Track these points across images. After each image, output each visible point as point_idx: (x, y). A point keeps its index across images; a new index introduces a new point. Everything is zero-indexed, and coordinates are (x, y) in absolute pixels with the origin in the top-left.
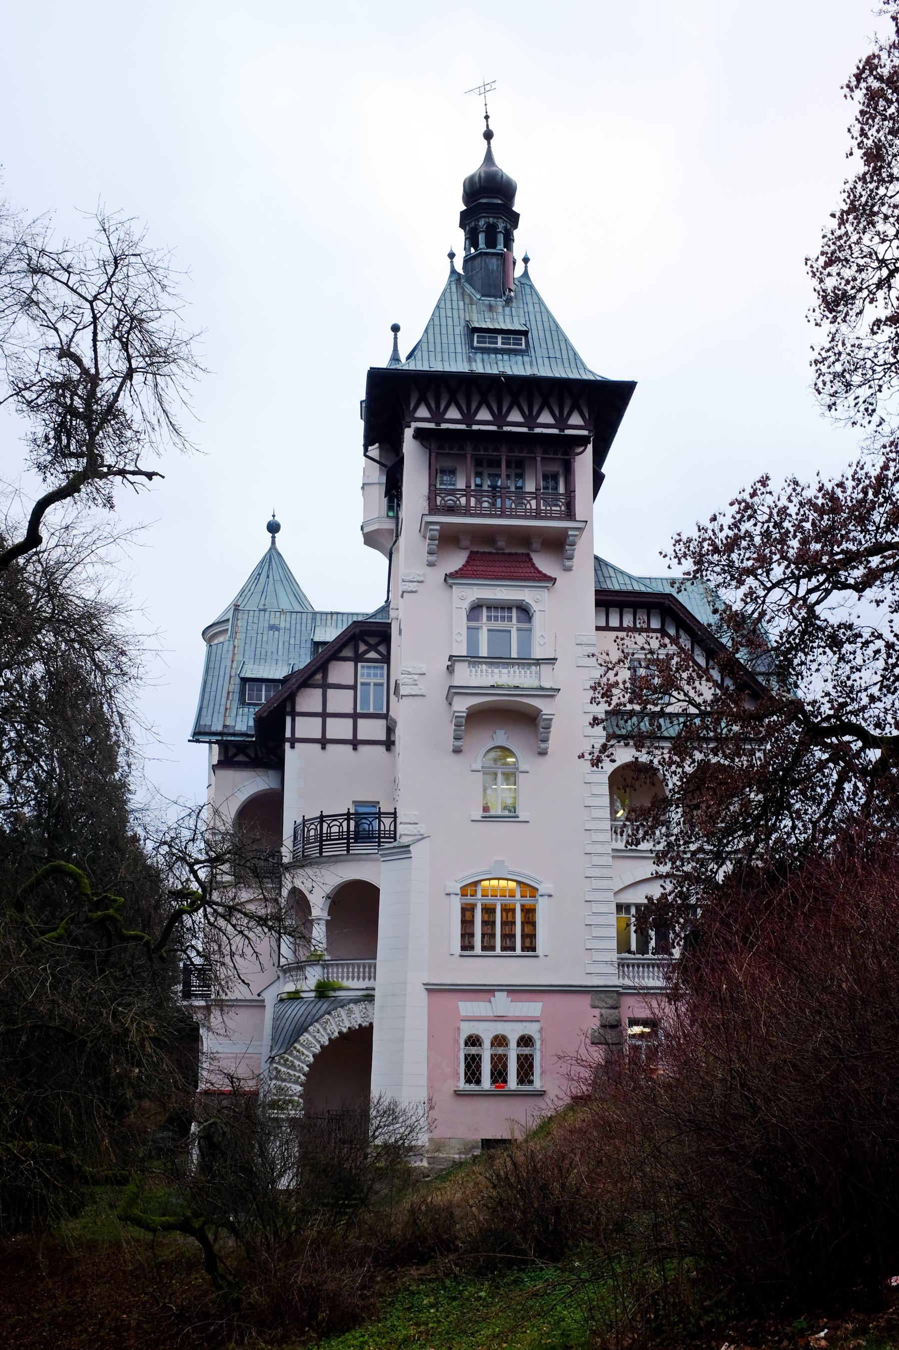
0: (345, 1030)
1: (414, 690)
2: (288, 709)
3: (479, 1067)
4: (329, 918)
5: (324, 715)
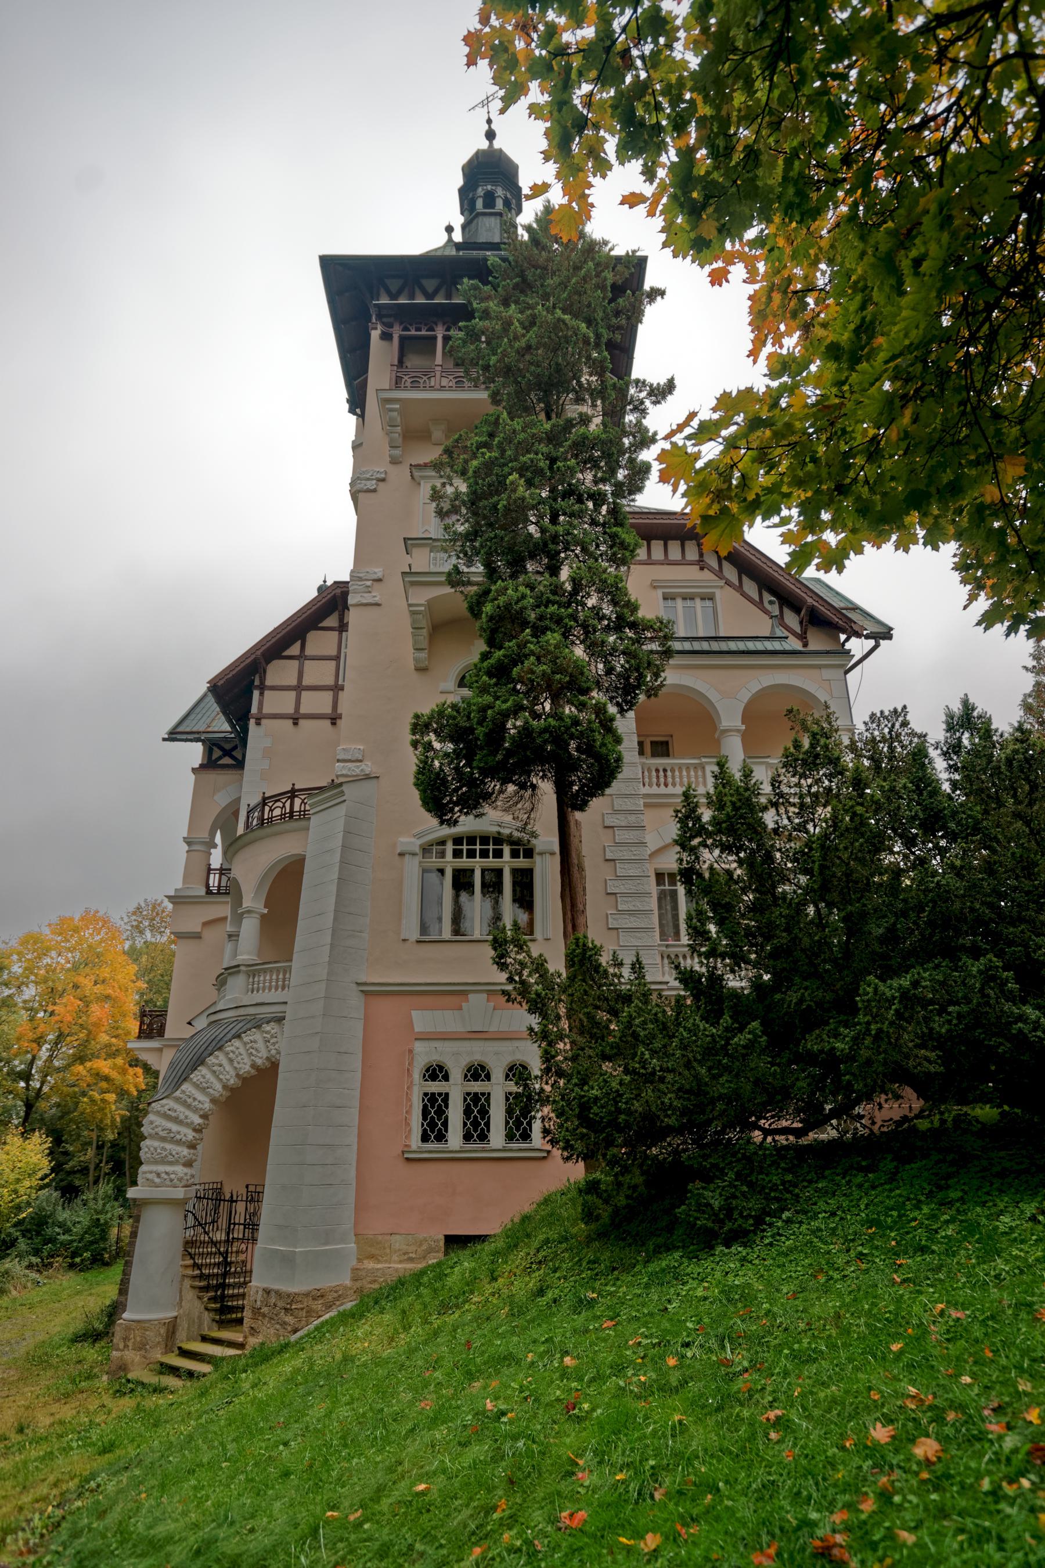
0: (259, 1062)
1: (368, 598)
2: (257, 683)
3: (484, 1112)
4: (266, 911)
5: (299, 688)
